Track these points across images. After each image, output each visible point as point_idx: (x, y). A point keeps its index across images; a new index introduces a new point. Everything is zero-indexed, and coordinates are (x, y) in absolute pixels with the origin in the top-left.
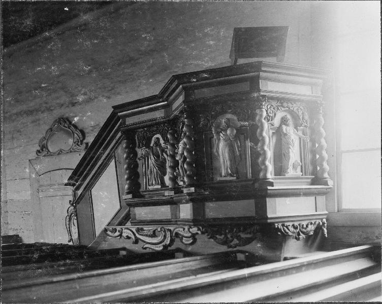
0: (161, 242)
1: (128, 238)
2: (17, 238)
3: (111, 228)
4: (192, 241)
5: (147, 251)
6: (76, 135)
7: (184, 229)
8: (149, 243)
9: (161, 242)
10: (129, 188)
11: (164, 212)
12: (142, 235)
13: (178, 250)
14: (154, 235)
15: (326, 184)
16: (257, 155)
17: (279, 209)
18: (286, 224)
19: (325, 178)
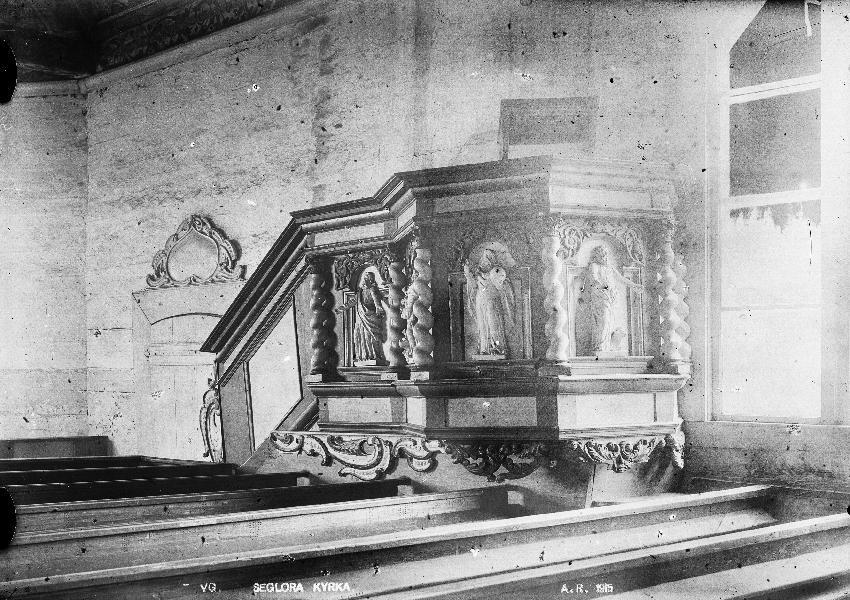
0: (374, 465)
1: (314, 454)
2: (103, 443)
3: (282, 434)
4: (428, 465)
5: (348, 480)
6: (223, 251)
7: (415, 443)
8: (352, 466)
9: (374, 465)
10: (316, 364)
11: (378, 409)
12: (340, 450)
13: (406, 481)
14: (361, 451)
15: (674, 371)
16: (543, 316)
17: (577, 416)
18: (593, 443)
19: (675, 361)
